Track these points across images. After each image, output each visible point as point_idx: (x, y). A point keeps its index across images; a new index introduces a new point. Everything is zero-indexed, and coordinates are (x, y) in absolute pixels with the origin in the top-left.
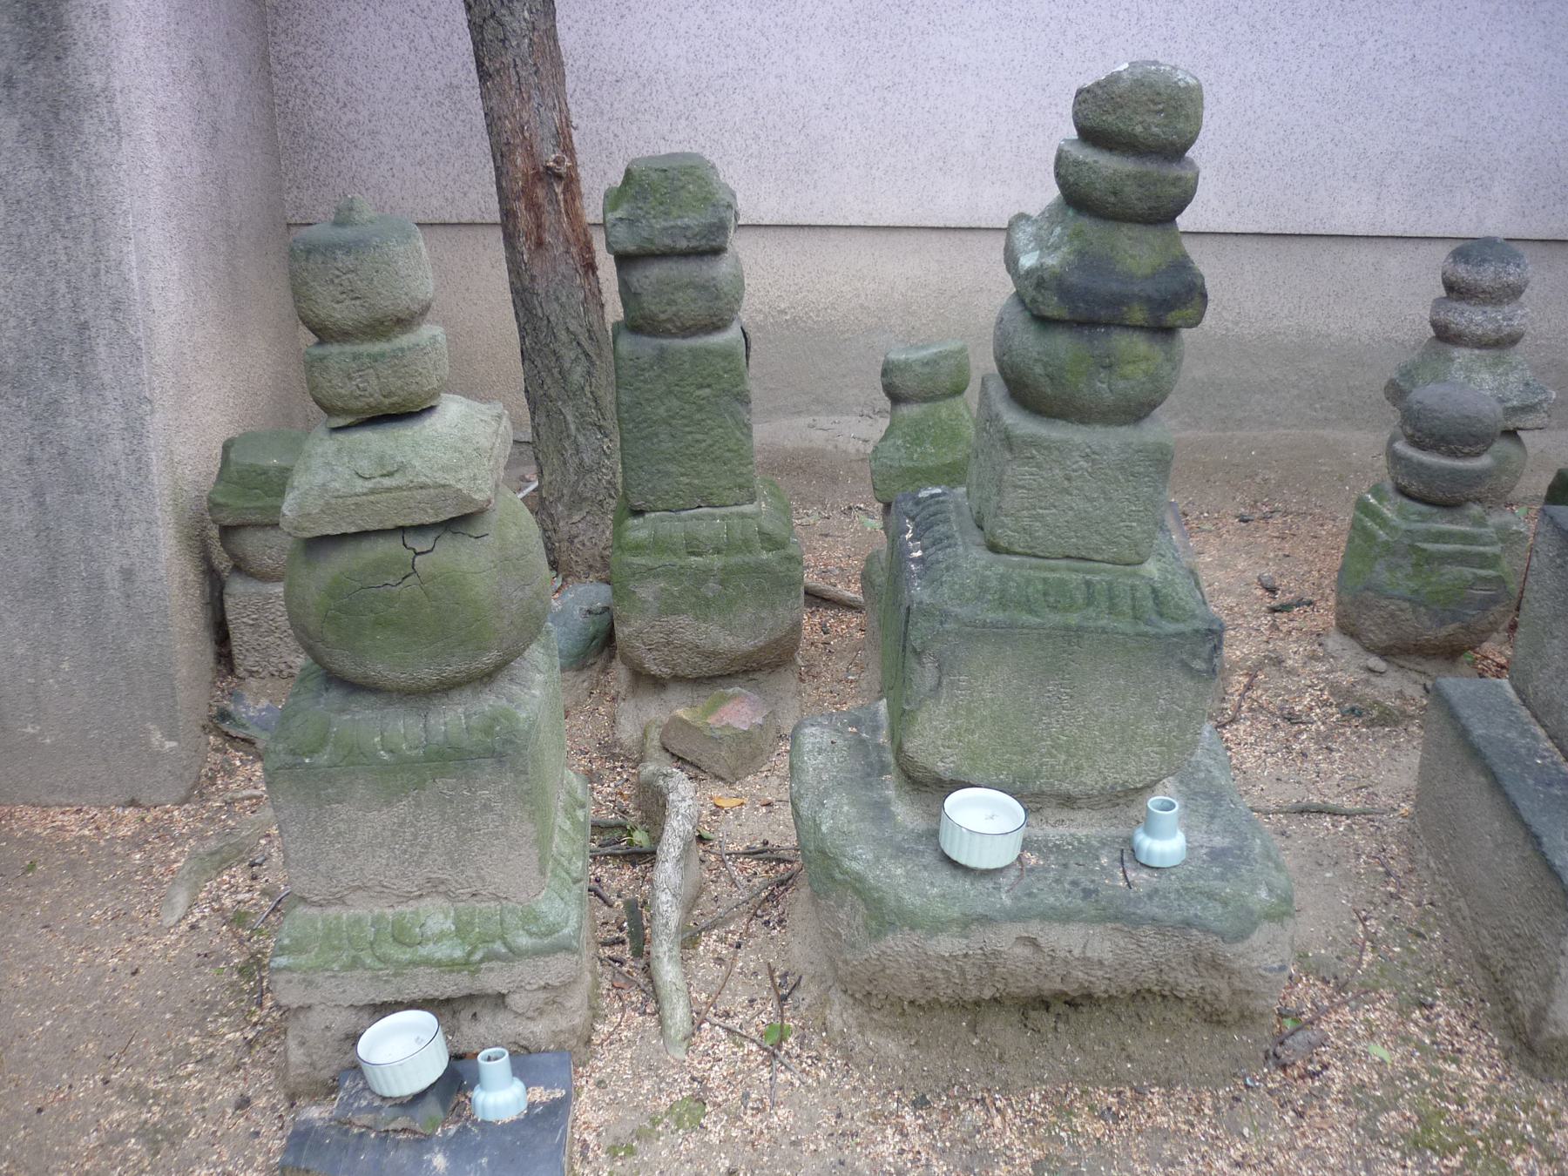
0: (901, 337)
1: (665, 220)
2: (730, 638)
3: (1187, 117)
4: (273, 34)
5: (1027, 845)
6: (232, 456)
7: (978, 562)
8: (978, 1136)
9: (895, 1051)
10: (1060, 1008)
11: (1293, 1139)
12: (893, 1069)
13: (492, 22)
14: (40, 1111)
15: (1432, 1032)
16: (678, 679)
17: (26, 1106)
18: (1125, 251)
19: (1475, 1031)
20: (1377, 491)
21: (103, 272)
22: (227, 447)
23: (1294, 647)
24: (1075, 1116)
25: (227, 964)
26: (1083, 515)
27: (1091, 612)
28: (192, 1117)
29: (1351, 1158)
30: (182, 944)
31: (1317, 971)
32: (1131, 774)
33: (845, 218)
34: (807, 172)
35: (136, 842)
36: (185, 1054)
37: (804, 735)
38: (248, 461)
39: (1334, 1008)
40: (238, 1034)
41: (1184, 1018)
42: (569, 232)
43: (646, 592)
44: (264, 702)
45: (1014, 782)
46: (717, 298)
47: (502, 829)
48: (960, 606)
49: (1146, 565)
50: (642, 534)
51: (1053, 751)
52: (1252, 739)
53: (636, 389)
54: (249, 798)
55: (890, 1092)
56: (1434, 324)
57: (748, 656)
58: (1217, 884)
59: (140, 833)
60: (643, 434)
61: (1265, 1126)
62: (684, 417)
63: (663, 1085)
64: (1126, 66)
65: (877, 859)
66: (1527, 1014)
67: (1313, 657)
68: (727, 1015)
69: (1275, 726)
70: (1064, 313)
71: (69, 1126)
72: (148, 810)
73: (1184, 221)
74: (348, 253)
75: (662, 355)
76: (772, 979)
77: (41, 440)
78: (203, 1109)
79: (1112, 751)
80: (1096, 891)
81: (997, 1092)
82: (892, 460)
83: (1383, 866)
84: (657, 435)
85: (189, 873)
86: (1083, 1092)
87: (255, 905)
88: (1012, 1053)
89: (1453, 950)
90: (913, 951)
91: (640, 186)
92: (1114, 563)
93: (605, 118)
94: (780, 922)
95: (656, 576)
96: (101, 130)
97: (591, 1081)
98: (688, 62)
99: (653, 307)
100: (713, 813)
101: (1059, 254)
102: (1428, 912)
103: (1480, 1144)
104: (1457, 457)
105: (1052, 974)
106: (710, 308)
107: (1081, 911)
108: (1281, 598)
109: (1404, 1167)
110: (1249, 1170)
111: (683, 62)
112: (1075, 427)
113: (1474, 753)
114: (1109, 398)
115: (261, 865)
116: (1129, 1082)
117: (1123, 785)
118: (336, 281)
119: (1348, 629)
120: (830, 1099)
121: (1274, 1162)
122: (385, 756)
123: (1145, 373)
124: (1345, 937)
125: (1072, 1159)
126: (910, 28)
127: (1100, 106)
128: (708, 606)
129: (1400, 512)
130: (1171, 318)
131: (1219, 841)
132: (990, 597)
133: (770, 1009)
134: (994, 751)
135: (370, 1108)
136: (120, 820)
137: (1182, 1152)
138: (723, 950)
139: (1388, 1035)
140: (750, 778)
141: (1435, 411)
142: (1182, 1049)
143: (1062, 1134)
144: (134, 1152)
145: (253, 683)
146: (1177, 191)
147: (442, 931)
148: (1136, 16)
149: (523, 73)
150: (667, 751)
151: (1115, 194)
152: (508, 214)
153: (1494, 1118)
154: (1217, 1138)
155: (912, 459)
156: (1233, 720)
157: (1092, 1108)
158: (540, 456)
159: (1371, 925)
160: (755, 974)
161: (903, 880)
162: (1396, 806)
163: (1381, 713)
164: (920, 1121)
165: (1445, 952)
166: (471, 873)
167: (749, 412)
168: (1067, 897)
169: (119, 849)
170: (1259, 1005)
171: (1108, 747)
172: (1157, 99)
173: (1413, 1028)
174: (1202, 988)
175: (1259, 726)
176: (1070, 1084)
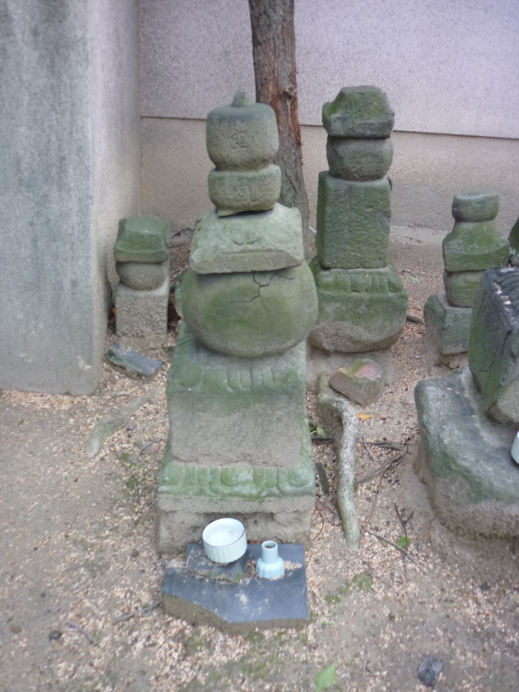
0: (432, 189)
1: (361, 120)
2: (368, 334)
4: (142, 22)
6: (127, 227)
12: (469, 567)
13: (264, 16)
14: (36, 549)
16: (337, 352)
17: (29, 546)
21: (74, 132)
22: (122, 225)
25: (121, 479)
28: (110, 559)
30: (97, 468)
33: (413, 127)
34: (396, 103)
35: (70, 413)
36: (104, 525)
37: (428, 390)
38: (134, 230)
40: (129, 517)
42: (291, 126)
44: (130, 349)
46: (382, 162)
47: (285, 431)
53: (335, 206)
54: (124, 395)
57: (375, 344)
59: (72, 409)
60: (336, 229)
62: (357, 222)
63: (349, 565)
65: (477, 461)
71: (50, 558)
72: (75, 397)
74: (243, 121)
76: (397, 511)
77: (38, 214)
78: (115, 555)
82: (457, 250)
84: (342, 230)
85: (99, 431)
87: (131, 450)
91: (349, 101)
94: (397, 481)
95: (336, 301)
96: (79, 59)
97: (312, 559)
98: (343, 44)
115: (132, 430)
118: (235, 137)
122: (230, 390)
126: (456, 32)
128: (360, 318)
133: (398, 528)
135: (206, 567)
136: (61, 402)
140: (373, 405)
144: (84, 575)
145: (124, 339)
147: (246, 480)
149: (277, 43)
155: (467, 251)
160: (387, 508)
161: (492, 474)
166: (265, 452)
167: (389, 222)
169: (62, 416)
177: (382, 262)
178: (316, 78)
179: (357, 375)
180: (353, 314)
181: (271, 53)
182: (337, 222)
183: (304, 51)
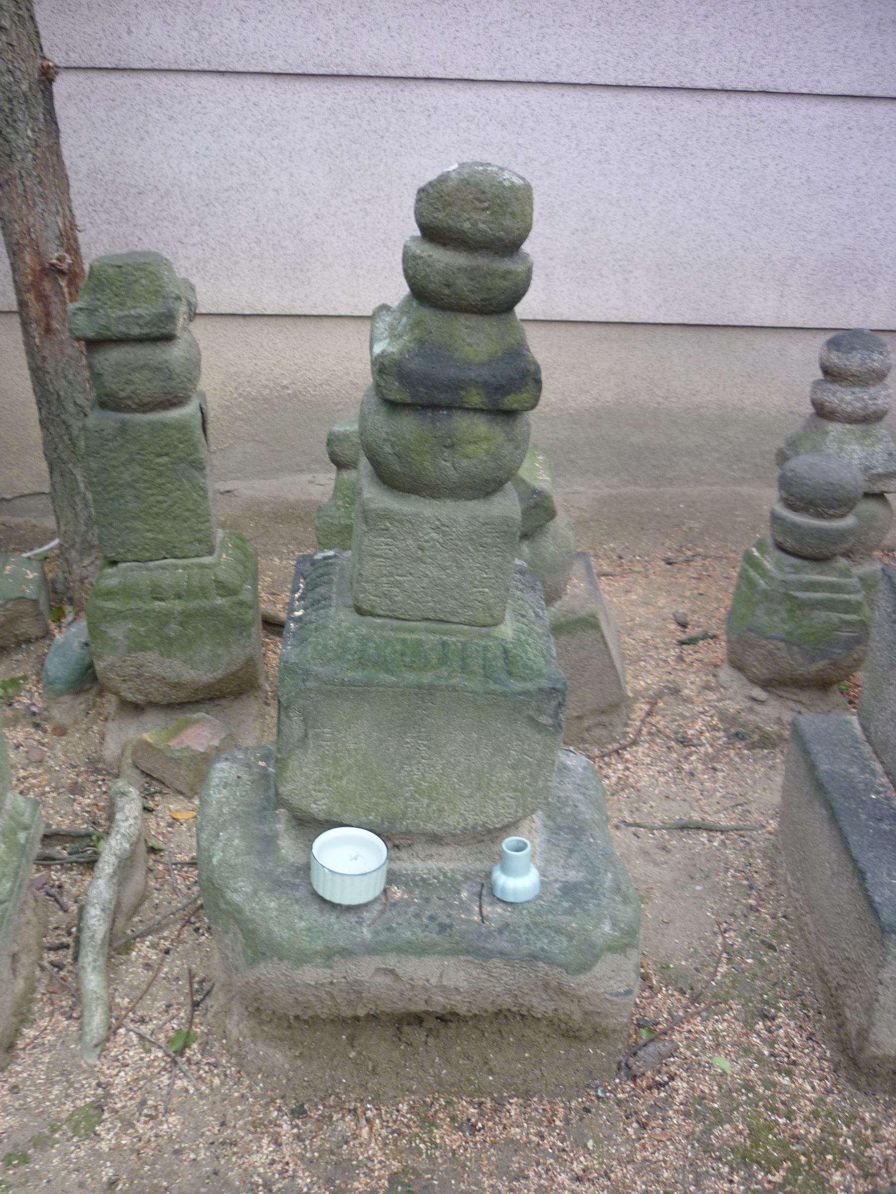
1: (121, 310)
2: (192, 672)
3: (513, 214)
5: (392, 878)
7: (344, 624)
8: (345, 1147)
9: (281, 1061)
10: (432, 1023)
11: (633, 1151)
15: (771, 1043)
16: (153, 705)
18: (464, 340)
19: (810, 1043)
20: (760, 546)
23: (692, 677)
24: (437, 1128)
26: (438, 582)
27: (444, 672)
29: (683, 1172)
31: (676, 982)
32: (490, 816)
33: (335, 309)
34: (302, 270)
39: (689, 1017)
41: (541, 1035)
43: (117, 632)
45: (383, 823)
46: (170, 378)
48: (322, 665)
49: (502, 627)
50: (113, 582)
51: (417, 795)
52: (648, 760)
53: (103, 457)
55: (273, 1101)
56: (814, 403)
57: (210, 686)
58: (565, 918)
61: (609, 1138)
62: (146, 481)
63: (71, 1091)
64: (456, 166)
65: (255, 892)
66: (853, 1034)
67: (707, 687)
68: (142, 1021)
69: (669, 748)
70: (408, 398)
73: (522, 310)
75: (123, 428)
76: (191, 984)
79: (471, 796)
80: (451, 926)
81: (369, 1102)
82: (333, 518)
83: (747, 879)
84: (122, 497)
86: (447, 1102)
88: (384, 1066)
89: (798, 963)
90: (282, 978)
91: (99, 280)
92: (470, 625)
93: (131, 224)
95: (125, 618)
98: (198, 177)
99: (113, 386)
100: (170, 825)
101: (401, 342)
102: (781, 925)
103: (803, 1159)
104: (824, 518)
105: (416, 999)
106: (164, 386)
107: (436, 945)
108: (691, 632)
109: (731, 1182)
110: (587, 1184)
111: (194, 178)
112: (427, 501)
113: (819, 787)
114: (454, 475)
116: (490, 1094)
117: (483, 826)
119: (738, 665)
120: (219, 1106)
121: (612, 1176)
123: (487, 452)
124: (705, 948)
125: (427, 1171)
127: (431, 204)
128: (171, 644)
129: (778, 564)
130: (509, 401)
131: (574, 876)
132: (350, 657)
134: (361, 796)
137: (529, 1165)
138: (154, 956)
139: (732, 1046)
141: (805, 478)
142: (540, 1063)
143: (422, 1146)
146: (506, 283)
148: (575, 142)
149: (28, 183)
150: (137, 767)
151: (448, 286)
152: (22, 304)
153: (819, 1131)
154: (564, 1150)
156: (634, 743)
157: (453, 1119)
158: (57, 510)
159: (730, 937)
160: (177, 979)
161: (275, 913)
162: (764, 823)
163: (761, 737)
164: (295, 1131)
165: (792, 964)
167: (204, 477)
168: (423, 931)
170: (611, 1023)
171: (467, 792)
172: (482, 197)
173: (755, 1040)
174: (556, 1010)
175: (656, 748)
176: (436, 1095)
177: (203, 546)
178: (159, 233)
179: (173, 743)
180: (158, 639)
181: (19, 201)
182: (111, 484)
183: (133, 191)
